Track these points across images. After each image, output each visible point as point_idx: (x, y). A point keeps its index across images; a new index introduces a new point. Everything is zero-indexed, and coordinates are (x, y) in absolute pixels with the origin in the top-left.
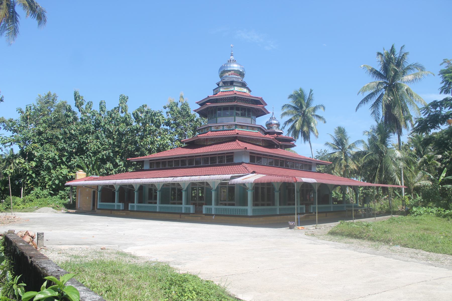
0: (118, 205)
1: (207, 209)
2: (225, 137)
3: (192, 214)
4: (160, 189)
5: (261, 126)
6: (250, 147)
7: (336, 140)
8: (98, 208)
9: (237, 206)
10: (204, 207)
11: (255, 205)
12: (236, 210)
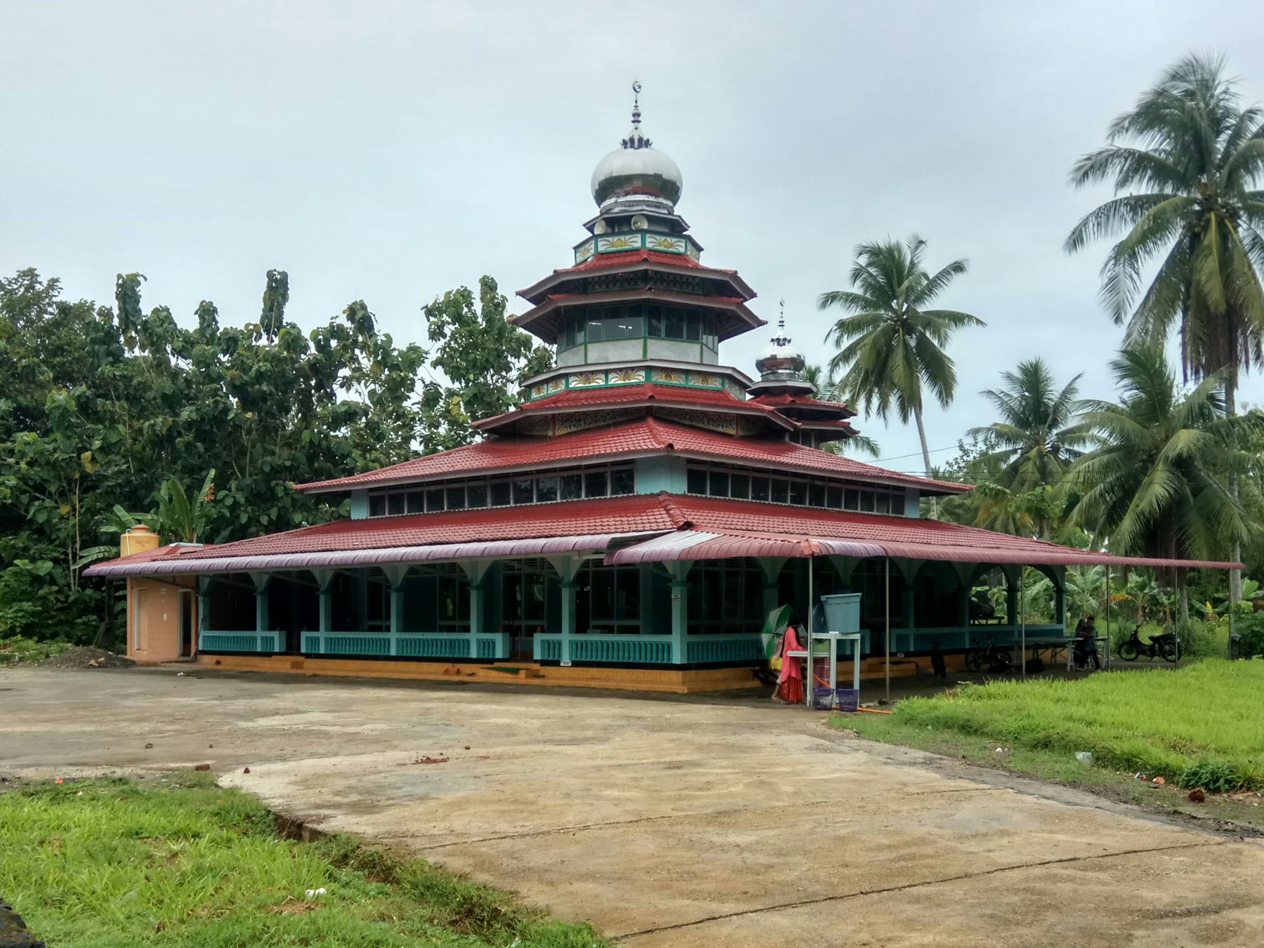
0: (311, 638)
1: (546, 645)
2: (613, 411)
3: (277, 654)
4: (264, 585)
5: (734, 369)
6: (684, 442)
7: (1011, 412)
8: (200, 648)
9: (646, 632)
10: (538, 638)
11: (692, 630)
12: (660, 647)
